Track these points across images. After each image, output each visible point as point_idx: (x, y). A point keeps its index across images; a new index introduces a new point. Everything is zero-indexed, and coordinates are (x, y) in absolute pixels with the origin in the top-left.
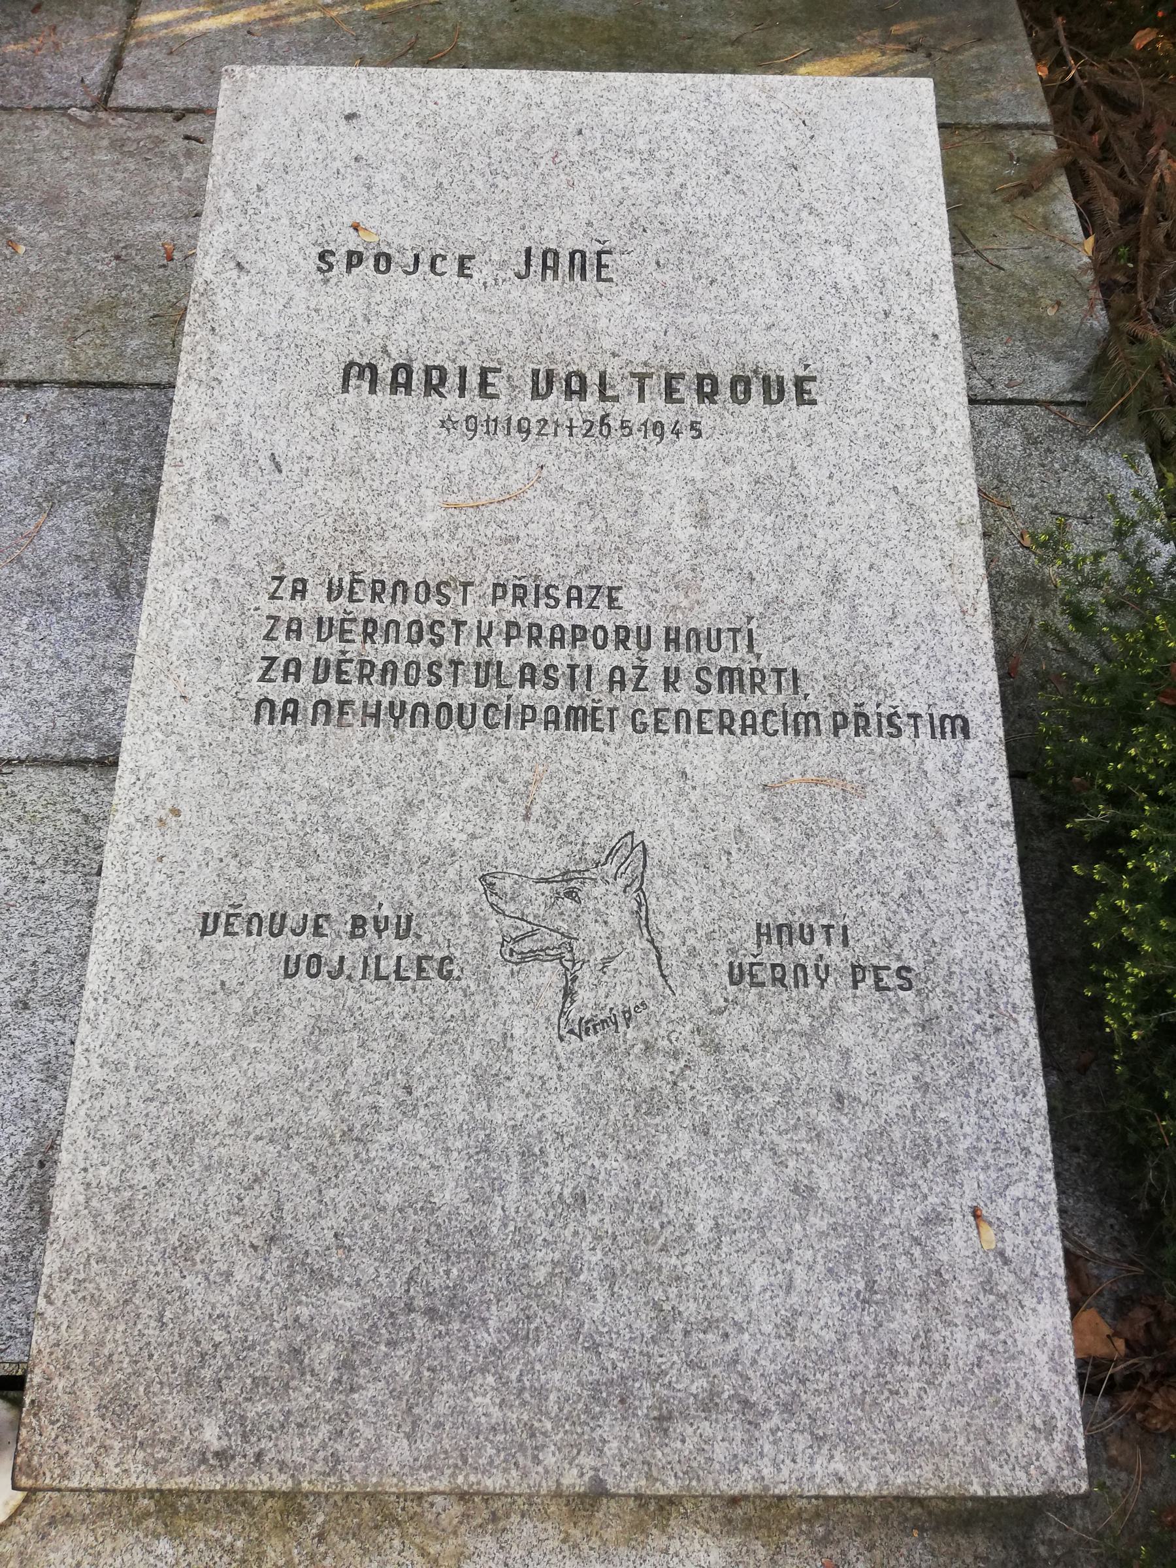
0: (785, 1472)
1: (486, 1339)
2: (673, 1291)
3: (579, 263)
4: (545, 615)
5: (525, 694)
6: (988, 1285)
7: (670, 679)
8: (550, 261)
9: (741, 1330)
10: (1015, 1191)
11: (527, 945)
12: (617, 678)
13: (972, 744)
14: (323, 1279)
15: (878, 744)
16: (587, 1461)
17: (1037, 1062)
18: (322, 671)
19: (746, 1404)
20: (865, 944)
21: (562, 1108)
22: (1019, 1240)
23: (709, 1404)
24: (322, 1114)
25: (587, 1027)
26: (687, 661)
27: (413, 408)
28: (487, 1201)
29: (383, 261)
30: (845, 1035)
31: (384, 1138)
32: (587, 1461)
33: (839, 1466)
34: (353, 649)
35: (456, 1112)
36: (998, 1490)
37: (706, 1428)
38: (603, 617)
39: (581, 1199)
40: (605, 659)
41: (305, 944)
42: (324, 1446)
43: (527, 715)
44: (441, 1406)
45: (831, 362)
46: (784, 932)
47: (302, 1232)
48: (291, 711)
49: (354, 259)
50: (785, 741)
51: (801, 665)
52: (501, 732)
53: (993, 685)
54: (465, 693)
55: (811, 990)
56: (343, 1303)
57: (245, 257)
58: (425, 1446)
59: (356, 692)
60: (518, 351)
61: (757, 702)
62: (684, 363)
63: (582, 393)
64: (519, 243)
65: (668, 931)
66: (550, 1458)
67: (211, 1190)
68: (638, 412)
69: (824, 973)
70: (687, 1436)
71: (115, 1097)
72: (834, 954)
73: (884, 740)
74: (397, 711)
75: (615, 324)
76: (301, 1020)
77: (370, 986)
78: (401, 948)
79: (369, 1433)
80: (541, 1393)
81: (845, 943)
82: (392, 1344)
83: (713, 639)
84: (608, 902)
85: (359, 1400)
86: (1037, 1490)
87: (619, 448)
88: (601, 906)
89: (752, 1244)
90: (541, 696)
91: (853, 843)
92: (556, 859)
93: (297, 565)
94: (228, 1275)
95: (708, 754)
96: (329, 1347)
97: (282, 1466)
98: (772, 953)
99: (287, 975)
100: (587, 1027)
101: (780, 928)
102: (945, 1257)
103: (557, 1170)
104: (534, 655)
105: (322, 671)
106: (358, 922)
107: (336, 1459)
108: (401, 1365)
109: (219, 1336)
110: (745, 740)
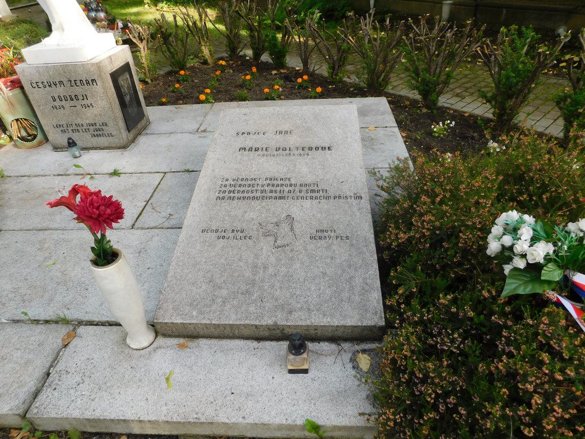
0: (317, 321)
1: (253, 298)
2: (294, 290)
3: (286, 132)
4: (275, 182)
5: (270, 194)
6: (363, 289)
7: (300, 191)
8: (281, 132)
9: (309, 297)
10: (370, 273)
11: (267, 234)
12: (289, 192)
13: (363, 200)
14: (220, 288)
15: (343, 201)
16: (273, 319)
17: (375, 251)
18: (230, 192)
19: (309, 309)
20: (339, 232)
21: (273, 259)
22: (370, 281)
23: (301, 309)
24: (223, 261)
25: (279, 247)
26: (304, 189)
27: (252, 153)
28: (255, 275)
29: (249, 133)
30: (334, 247)
31: (235, 265)
32: (273, 319)
33: (329, 320)
34: (236, 189)
35: (250, 261)
36: (364, 324)
37: (300, 313)
38: (287, 182)
39: (275, 275)
40: (286, 189)
41: (221, 234)
42: (218, 316)
43: (270, 198)
44: (243, 309)
45: (335, 144)
46: (322, 231)
47: (217, 281)
48: (223, 198)
49: (243, 133)
50: (323, 200)
51: (327, 189)
52: (265, 200)
53: (375, 248)
54: (259, 194)
55: (327, 240)
56: (224, 292)
57: (222, 134)
58: (239, 316)
59: (236, 195)
60: (273, 144)
61: (318, 195)
62: (307, 145)
63: (286, 150)
64: (275, 131)
65: (297, 231)
66: (265, 318)
67: (199, 273)
68: (296, 152)
69: (330, 237)
70: (295, 315)
71: (182, 258)
72: (332, 234)
73: (344, 200)
74: (244, 198)
75: (293, 140)
76: (220, 246)
77: (235, 241)
78: (241, 235)
79: (227, 314)
80: (264, 307)
81: (335, 232)
82: (234, 299)
83: (310, 185)
84: (285, 228)
85: (226, 308)
86: (373, 324)
87: (292, 158)
88: (283, 227)
89: (312, 282)
90: (274, 195)
91: (337, 216)
92: (275, 220)
93: (226, 176)
94: (201, 287)
95: (307, 203)
96: (220, 299)
97: (209, 319)
98: (319, 234)
99: (218, 239)
100: (279, 247)
101: (321, 231)
102: (354, 284)
103: (271, 270)
104: (273, 188)
105: (230, 192)
106: (233, 231)
107: (220, 318)
108: (235, 303)
109: (198, 297)
110: (315, 201)
